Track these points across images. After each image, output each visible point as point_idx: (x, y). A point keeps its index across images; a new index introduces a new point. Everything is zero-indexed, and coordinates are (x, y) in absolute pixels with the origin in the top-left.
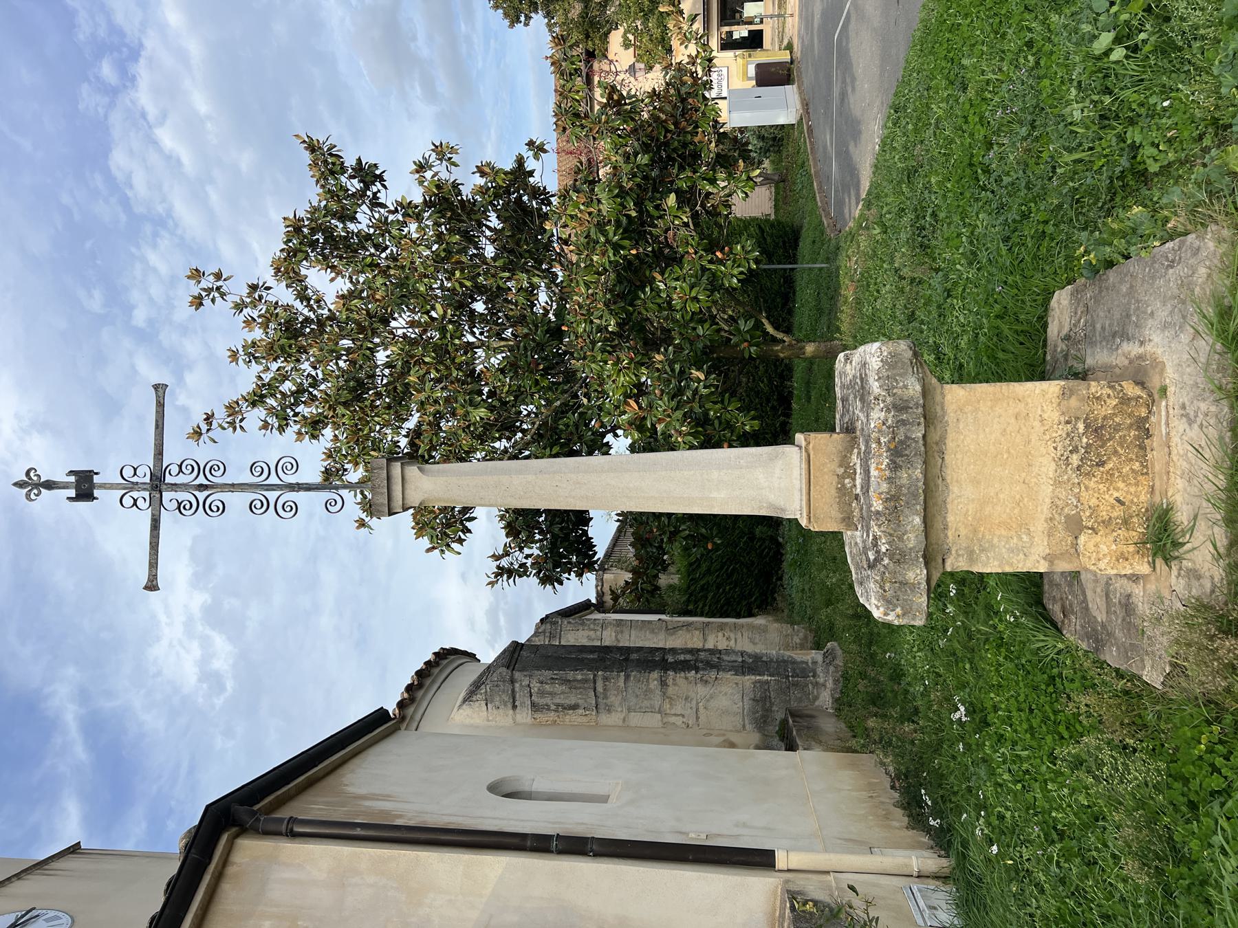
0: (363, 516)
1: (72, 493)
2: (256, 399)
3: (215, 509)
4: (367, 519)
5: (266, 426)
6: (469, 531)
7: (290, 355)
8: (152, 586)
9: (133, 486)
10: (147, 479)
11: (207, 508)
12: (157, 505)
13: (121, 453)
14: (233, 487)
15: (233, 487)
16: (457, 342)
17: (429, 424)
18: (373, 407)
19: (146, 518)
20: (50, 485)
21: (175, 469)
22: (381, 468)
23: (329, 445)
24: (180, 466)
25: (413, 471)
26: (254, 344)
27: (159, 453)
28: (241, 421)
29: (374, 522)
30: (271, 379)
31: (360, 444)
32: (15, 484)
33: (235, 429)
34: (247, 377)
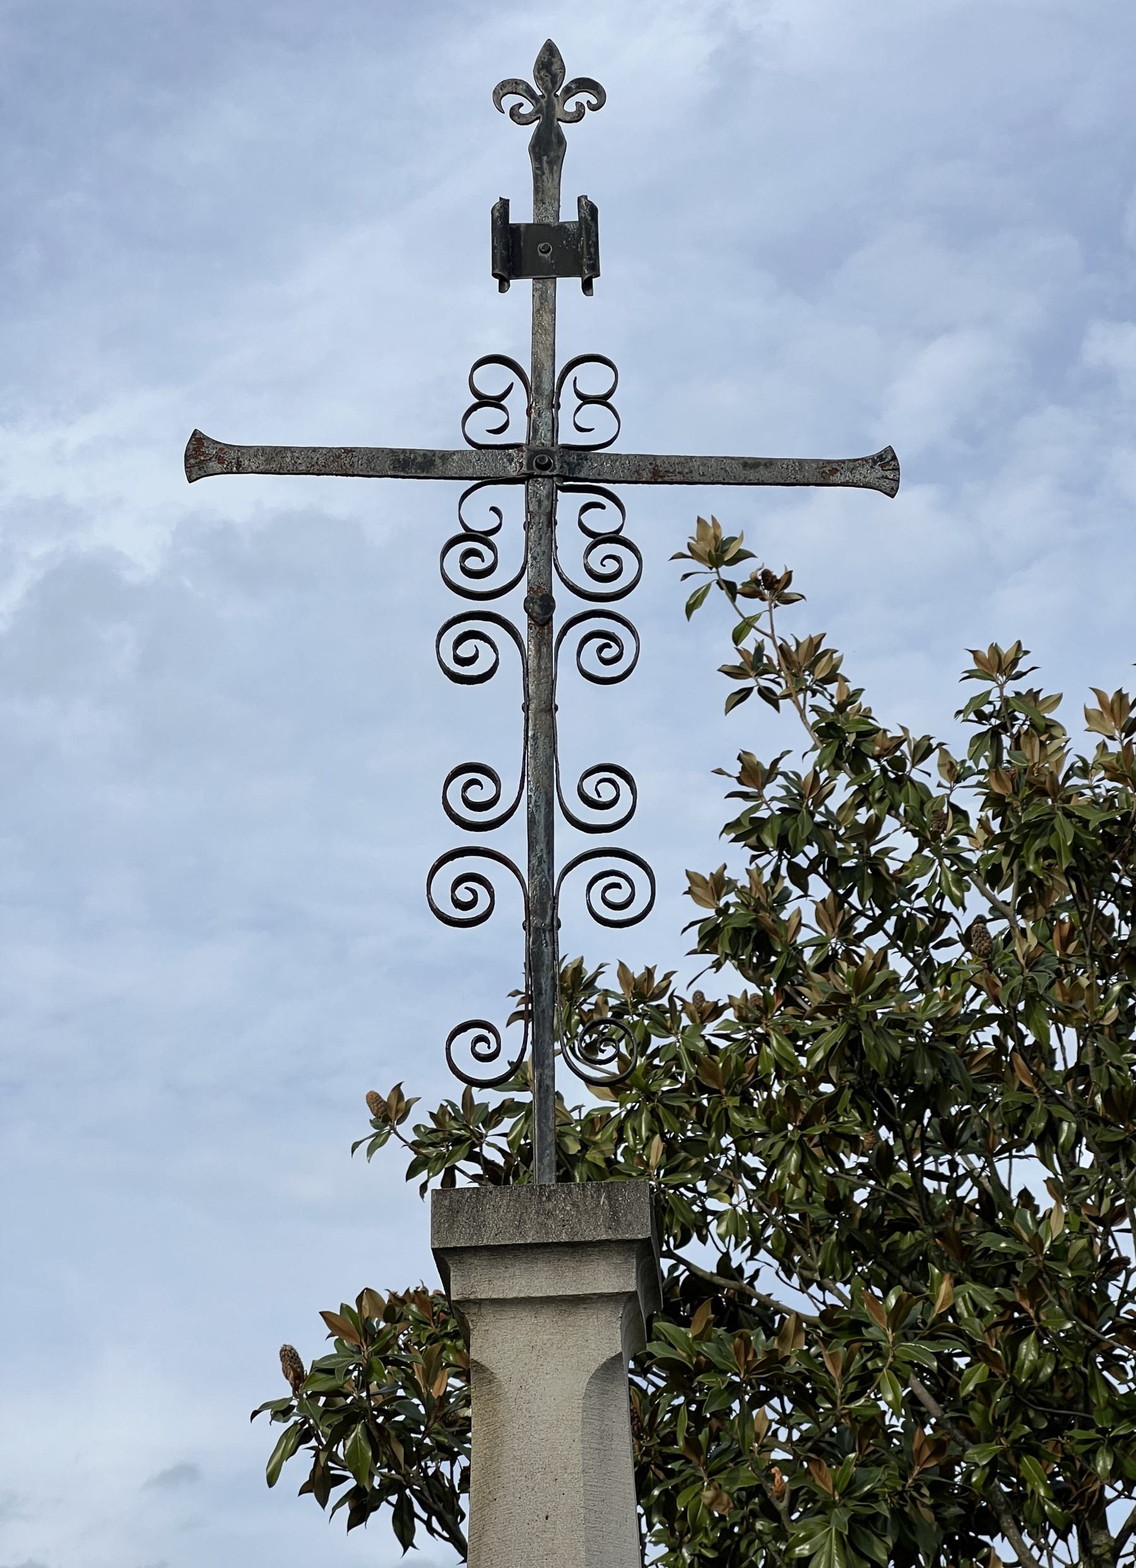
0: (420, 1116)
1: (522, 214)
2: (847, 738)
3: (466, 650)
4: (406, 1130)
5: (754, 775)
6: (358, 1517)
7: (1015, 851)
8: (204, 457)
9: (544, 398)
10: (568, 436)
11: (467, 627)
12: (482, 467)
13: (659, 356)
14: (541, 712)
15: (541, 712)
16: (1103, 1463)
17: (774, 1360)
18: (832, 1144)
19: (439, 435)
20: (547, 150)
21: (603, 520)
22: (614, 1219)
23: (681, 988)
24: (615, 538)
25: (603, 1337)
26: (1046, 730)
27: (658, 471)
28: (767, 695)
29: (397, 1154)
30: (923, 789)
31: (693, 1099)
32: (550, 49)
33: (735, 673)
34: (920, 701)
